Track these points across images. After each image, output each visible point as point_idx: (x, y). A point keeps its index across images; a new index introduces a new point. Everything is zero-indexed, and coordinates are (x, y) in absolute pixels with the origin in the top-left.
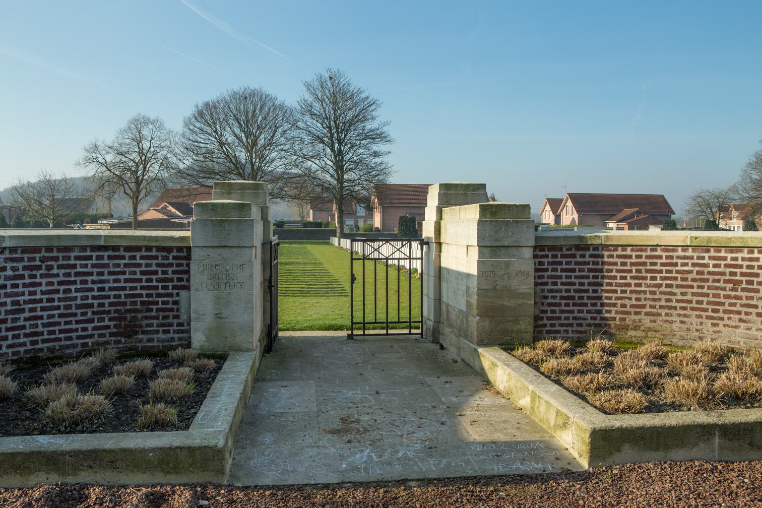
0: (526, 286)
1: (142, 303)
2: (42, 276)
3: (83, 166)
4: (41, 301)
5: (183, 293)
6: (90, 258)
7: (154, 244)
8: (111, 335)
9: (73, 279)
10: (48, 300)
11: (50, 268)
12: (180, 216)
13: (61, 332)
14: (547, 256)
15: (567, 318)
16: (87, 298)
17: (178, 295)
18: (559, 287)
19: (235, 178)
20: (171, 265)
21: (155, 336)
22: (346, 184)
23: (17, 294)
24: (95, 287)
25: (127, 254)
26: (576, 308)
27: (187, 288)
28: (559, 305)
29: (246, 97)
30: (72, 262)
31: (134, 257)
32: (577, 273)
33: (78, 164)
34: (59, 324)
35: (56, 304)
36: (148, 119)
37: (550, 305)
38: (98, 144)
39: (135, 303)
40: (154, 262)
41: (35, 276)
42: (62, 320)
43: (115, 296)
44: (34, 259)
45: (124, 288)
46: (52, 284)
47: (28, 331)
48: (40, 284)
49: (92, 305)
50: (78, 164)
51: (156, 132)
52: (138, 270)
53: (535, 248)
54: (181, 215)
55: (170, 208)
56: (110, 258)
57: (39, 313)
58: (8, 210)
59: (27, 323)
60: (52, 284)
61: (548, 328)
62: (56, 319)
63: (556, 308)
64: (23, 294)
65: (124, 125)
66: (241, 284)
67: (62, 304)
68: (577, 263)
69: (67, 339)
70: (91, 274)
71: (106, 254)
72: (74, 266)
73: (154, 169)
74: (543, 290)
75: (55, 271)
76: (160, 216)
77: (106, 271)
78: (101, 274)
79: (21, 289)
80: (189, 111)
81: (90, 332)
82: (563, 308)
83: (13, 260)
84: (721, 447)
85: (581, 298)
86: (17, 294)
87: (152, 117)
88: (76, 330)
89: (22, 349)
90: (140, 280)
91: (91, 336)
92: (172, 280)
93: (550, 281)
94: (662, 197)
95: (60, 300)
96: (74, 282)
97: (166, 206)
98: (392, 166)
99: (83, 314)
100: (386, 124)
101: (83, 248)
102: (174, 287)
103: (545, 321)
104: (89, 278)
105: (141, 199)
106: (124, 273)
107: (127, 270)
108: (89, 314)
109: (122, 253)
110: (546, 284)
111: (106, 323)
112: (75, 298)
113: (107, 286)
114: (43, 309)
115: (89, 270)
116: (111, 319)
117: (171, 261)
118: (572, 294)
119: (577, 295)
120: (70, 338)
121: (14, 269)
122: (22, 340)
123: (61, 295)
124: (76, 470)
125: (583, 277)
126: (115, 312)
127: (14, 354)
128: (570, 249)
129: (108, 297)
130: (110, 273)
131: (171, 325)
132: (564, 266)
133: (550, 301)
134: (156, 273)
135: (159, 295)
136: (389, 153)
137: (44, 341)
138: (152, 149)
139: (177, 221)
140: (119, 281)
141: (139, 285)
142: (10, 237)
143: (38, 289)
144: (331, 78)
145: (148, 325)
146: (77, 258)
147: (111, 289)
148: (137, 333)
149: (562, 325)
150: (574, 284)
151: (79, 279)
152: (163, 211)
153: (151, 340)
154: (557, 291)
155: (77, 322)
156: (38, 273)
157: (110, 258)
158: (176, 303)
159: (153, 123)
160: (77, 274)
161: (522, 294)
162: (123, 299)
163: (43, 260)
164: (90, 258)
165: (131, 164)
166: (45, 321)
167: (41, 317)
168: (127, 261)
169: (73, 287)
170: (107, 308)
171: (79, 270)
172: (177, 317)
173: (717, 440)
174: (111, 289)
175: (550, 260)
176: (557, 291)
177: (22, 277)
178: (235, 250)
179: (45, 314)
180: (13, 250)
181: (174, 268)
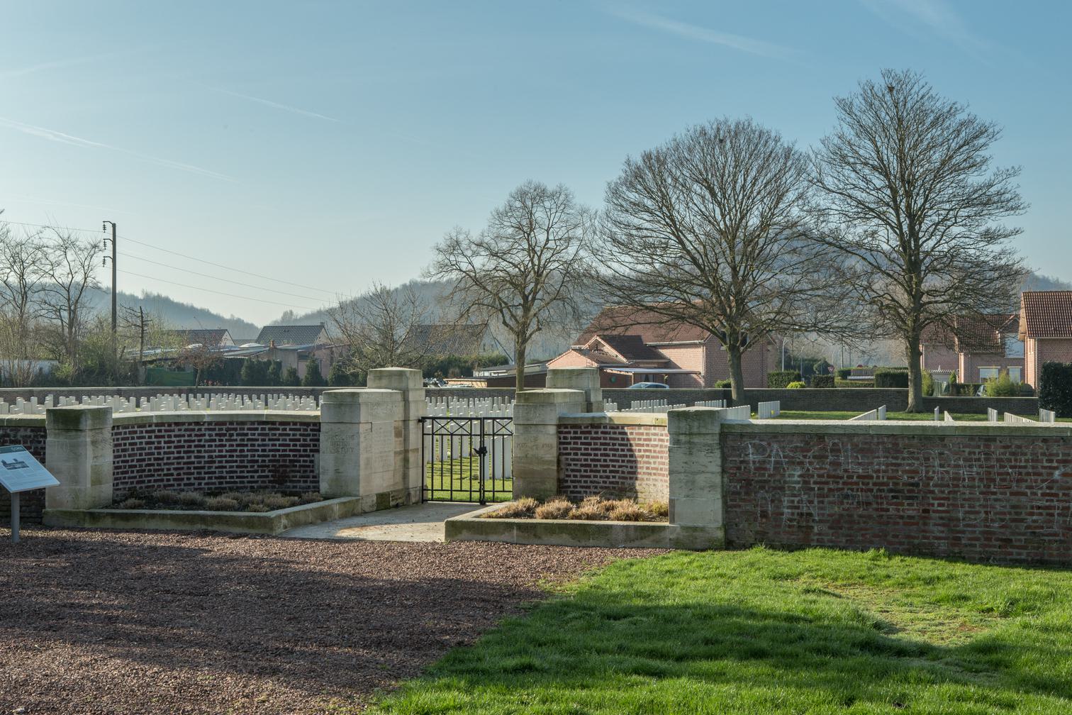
0: (551, 455)
1: (290, 461)
2: (227, 440)
4: (225, 456)
5: (316, 455)
6: (257, 429)
7: (298, 420)
8: (270, 482)
9: (246, 443)
10: (230, 456)
11: (231, 435)
13: (237, 477)
14: (570, 433)
15: (586, 482)
16: (254, 456)
17: (313, 456)
18: (579, 457)
20: (309, 435)
21: (298, 484)
22: (925, 299)
23: (211, 451)
24: (260, 449)
25: (281, 427)
26: (592, 474)
27: (318, 451)
28: (580, 471)
30: (245, 432)
31: (285, 429)
32: (593, 446)
34: (236, 472)
35: (235, 459)
36: (544, 191)
37: (572, 471)
38: (461, 237)
39: (285, 461)
40: (298, 433)
41: (222, 440)
42: (239, 470)
43: (273, 456)
44: (222, 429)
45: (278, 451)
46: (232, 445)
47: (217, 475)
48: (225, 446)
49: (257, 461)
51: (558, 214)
52: (288, 438)
53: (559, 426)
54: (624, 360)
55: (608, 349)
56: (270, 429)
57: (224, 464)
58: (328, 352)
59: (217, 470)
60: (232, 445)
61: (572, 489)
62: (235, 469)
63: (578, 474)
64: (215, 451)
66: (352, 449)
67: (238, 459)
68: (592, 438)
69: (241, 482)
70: (257, 440)
71: (267, 427)
72: (247, 435)
74: (567, 459)
75: (235, 437)
77: (267, 438)
78: (264, 440)
79: (213, 448)
81: (256, 479)
82: (583, 473)
83: (209, 429)
84: (517, 536)
85: (596, 466)
86: (211, 451)
88: (247, 477)
89: (213, 486)
90: (289, 445)
91: (257, 482)
92: (309, 445)
93: (572, 452)
95: (237, 456)
96: (247, 445)
99: (252, 467)
100: (1013, 172)
101: (253, 423)
102: (311, 451)
103: (569, 484)
104: (256, 443)
105: (531, 335)
106: (278, 440)
107: (281, 438)
108: (256, 467)
109: (278, 426)
110: (570, 454)
111: (266, 473)
112: (247, 456)
113: (267, 448)
114: (227, 462)
115: (256, 437)
116: (269, 471)
117: (309, 432)
118: (589, 462)
119: (593, 463)
120: (243, 482)
121: (210, 435)
122: (214, 481)
123: (238, 453)
124: (212, 524)
125: (596, 449)
126: (273, 466)
127: (209, 489)
128: (587, 427)
129: (268, 456)
130: (270, 440)
131: (308, 477)
132: (583, 441)
133: (572, 467)
134: (299, 440)
135: (301, 456)
137: (227, 483)
138: (551, 244)
139: (615, 371)
140: (275, 445)
141: (288, 448)
142: (209, 415)
143: (224, 449)
144: (891, 89)
145: (293, 477)
146: (249, 429)
147: (270, 451)
148: (286, 481)
149: (582, 487)
150: (590, 455)
151: (249, 443)
153: (295, 487)
154: (578, 460)
155: (248, 472)
156: (224, 438)
157: (270, 429)
158: (312, 461)
159: (552, 196)
160: (248, 440)
161: (547, 461)
162: (277, 458)
163: (228, 430)
164: (257, 429)
165: (514, 271)
166: (228, 470)
167: (225, 467)
168: (280, 432)
169: (246, 449)
170: (267, 464)
171: (250, 437)
172: (312, 471)
173: (515, 532)
174: (270, 451)
175: (572, 435)
176: (578, 460)
177: (215, 440)
178: (348, 425)
179: (228, 465)
180: (210, 423)
181: (311, 437)
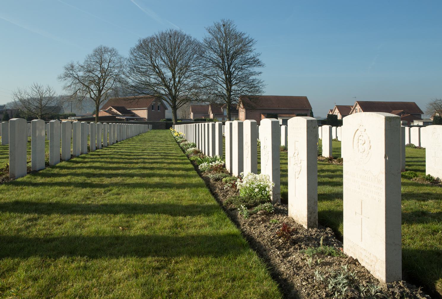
3: (63, 79)
12: (120, 115)
19: (29, 132)
29: (175, 35)
33: (60, 78)
50: (60, 78)
54: (121, 114)
55: (114, 110)
65: (91, 52)
73: (110, 83)
76: (107, 114)
80: (134, 43)
87: (110, 47)
94: (414, 103)
97: (111, 109)
98: (264, 81)
136: (261, 73)
144: (224, 25)
152: (109, 111)
